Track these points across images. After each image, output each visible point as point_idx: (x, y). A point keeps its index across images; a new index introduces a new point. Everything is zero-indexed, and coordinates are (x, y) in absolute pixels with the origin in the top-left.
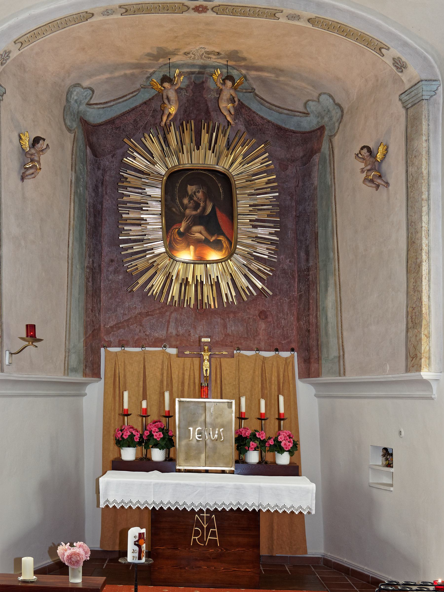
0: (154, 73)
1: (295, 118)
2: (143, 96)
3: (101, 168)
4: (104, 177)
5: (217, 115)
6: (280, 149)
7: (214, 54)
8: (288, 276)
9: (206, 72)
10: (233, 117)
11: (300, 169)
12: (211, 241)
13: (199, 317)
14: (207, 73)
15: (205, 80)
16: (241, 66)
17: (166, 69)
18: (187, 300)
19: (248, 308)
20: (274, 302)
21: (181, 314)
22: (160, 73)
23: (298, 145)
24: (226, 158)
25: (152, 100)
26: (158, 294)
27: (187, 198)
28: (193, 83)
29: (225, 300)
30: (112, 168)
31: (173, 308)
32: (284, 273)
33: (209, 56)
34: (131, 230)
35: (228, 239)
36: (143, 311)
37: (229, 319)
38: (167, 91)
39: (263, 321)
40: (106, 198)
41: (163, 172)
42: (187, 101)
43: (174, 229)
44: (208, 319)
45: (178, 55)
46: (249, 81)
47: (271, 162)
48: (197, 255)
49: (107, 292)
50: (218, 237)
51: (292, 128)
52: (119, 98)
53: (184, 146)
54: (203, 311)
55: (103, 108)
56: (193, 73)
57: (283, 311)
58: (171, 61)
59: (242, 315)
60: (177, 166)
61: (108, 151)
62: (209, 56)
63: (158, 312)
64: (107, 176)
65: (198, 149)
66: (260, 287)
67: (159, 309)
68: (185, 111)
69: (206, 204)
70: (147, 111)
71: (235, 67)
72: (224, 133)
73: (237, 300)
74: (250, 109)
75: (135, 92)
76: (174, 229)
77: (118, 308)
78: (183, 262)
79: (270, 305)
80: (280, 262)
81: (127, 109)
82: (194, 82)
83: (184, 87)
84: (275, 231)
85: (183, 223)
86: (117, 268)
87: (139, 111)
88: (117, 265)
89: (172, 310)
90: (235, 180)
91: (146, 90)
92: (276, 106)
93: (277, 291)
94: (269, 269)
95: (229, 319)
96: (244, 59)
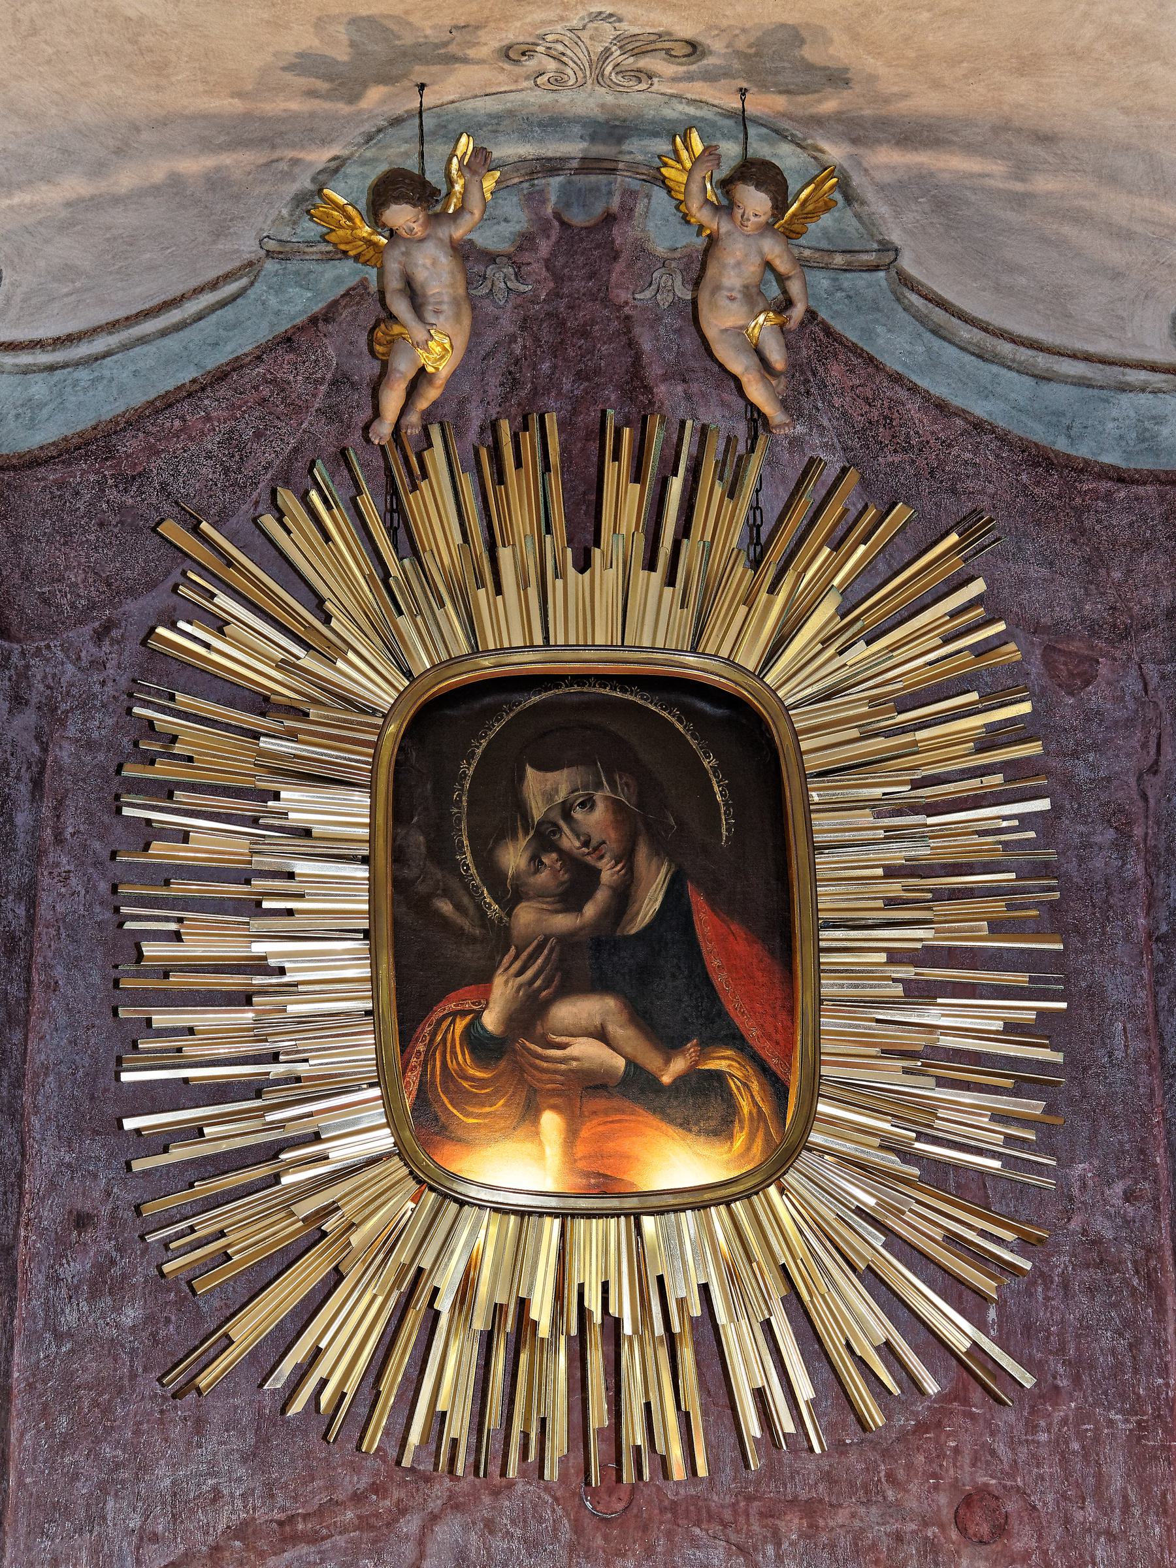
0: (336, 170)
1: (1125, 399)
2: (273, 301)
3: (34, 699)
4: (45, 750)
5: (688, 397)
6: (1044, 572)
7: (668, 51)
8: (1126, 1282)
9: (627, 158)
10: (781, 384)
11: (1163, 677)
12: (666, 1079)
13: (599, 1541)
14: (633, 167)
15: (622, 207)
16: (818, 121)
17: (404, 148)
18: (526, 1436)
19: (891, 1477)
20: (1043, 1437)
21: (490, 1526)
22: (364, 169)
23: (1148, 545)
24: (743, 609)
25: (327, 320)
26: (347, 1400)
27: (523, 842)
28: (556, 224)
29: (752, 1427)
30: (95, 696)
31: (440, 1489)
32: (1097, 1266)
33: (644, 63)
34: (191, 1031)
35: (764, 1069)
36: (261, 1516)
37: (778, 1545)
38: (407, 254)
39: (984, 1550)
40: (58, 865)
41: (385, 698)
42: (523, 328)
43: (445, 1017)
44: (649, 1551)
45: (465, 60)
46: (863, 203)
47: (1001, 627)
48: (580, 1165)
49: (45, 1406)
50: (703, 1056)
51: (1109, 459)
52: (137, 315)
53: (505, 555)
54: (620, 1506)
55: (51, 368)
56: (551, 166)
57: (1098, 1492)
58: (429, 99)
59: (857, 1523)
60: (460, 659)
61: (73, 606)
62: (644, 63)
63: (350, 1515)
64: (65, 744)
65: (584, 564)
66: (961, 1345)
67: (358, 1498)
68: (513, 382)
69: (630, 869)
70: (299, 386)
71: (785, 124)
72: (728, 474)
73: (830, 1430)
74: (870, 360)
75: (228, 277)
76: (445, 1017)
77: (110, 1504)
78: (501, 1210)
79: (1023, 1453)
80: (1071, 1199)
81: (186, 376)
82: (557, 216)
83: (505, 247)
84: (1041, 1012)
85: (498, 981)
86: (113, 1262)
87: (256, 388)
88: (109, 1246)
89: (434, 1505)
90: (796, 733)
91: (291, 266)
92: (1015, 340)
93: (1061, 1370)
94: (1009, 1236)
95: (778, 1545)
96: (838, 78)
